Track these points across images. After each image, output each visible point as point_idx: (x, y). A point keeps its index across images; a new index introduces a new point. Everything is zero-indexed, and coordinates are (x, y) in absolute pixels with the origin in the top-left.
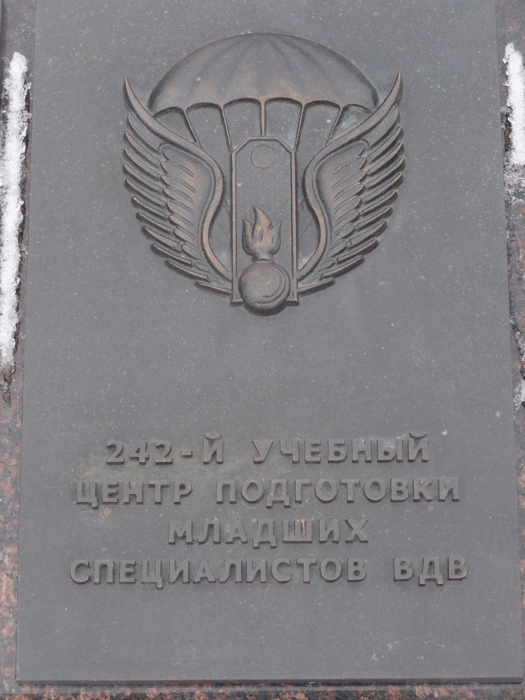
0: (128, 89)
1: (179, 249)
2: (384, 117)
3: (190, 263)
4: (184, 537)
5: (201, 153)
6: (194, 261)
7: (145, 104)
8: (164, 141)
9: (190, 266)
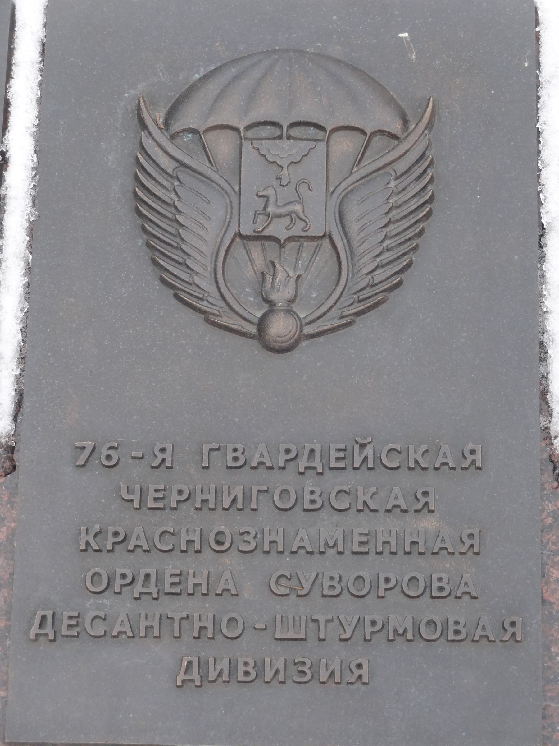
0: (145, 115)
1: (190, 281)
2: (413, 144)
3: (201, 296)
4: (335, 544)
5: (215, 177)
6: (206, 295)
9: (202, 299)
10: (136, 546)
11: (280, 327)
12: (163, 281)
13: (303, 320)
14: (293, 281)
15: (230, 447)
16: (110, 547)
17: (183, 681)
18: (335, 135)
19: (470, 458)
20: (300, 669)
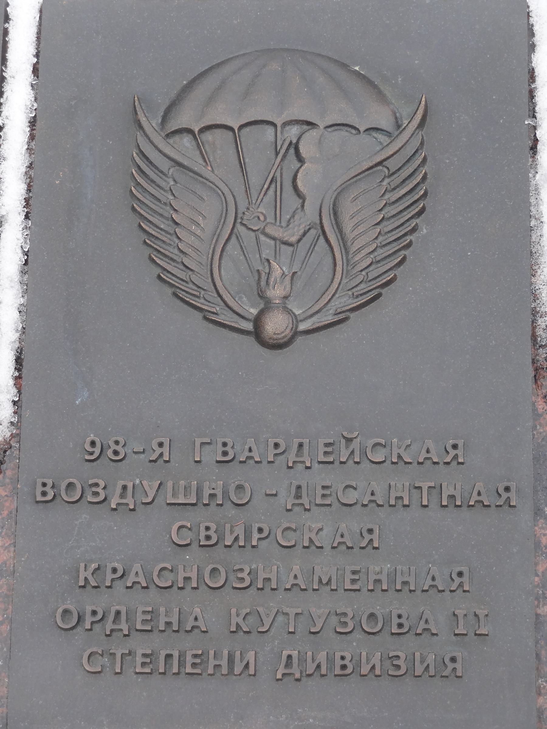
6: (203, 292)
7: (156, 122)
9: (198, 297)
11: (276, 325)
13: (298, 317)
14: (288, 279)
15: (220, 441)
17: (284, 675)
19: (452, 452)
20: (394, 663)
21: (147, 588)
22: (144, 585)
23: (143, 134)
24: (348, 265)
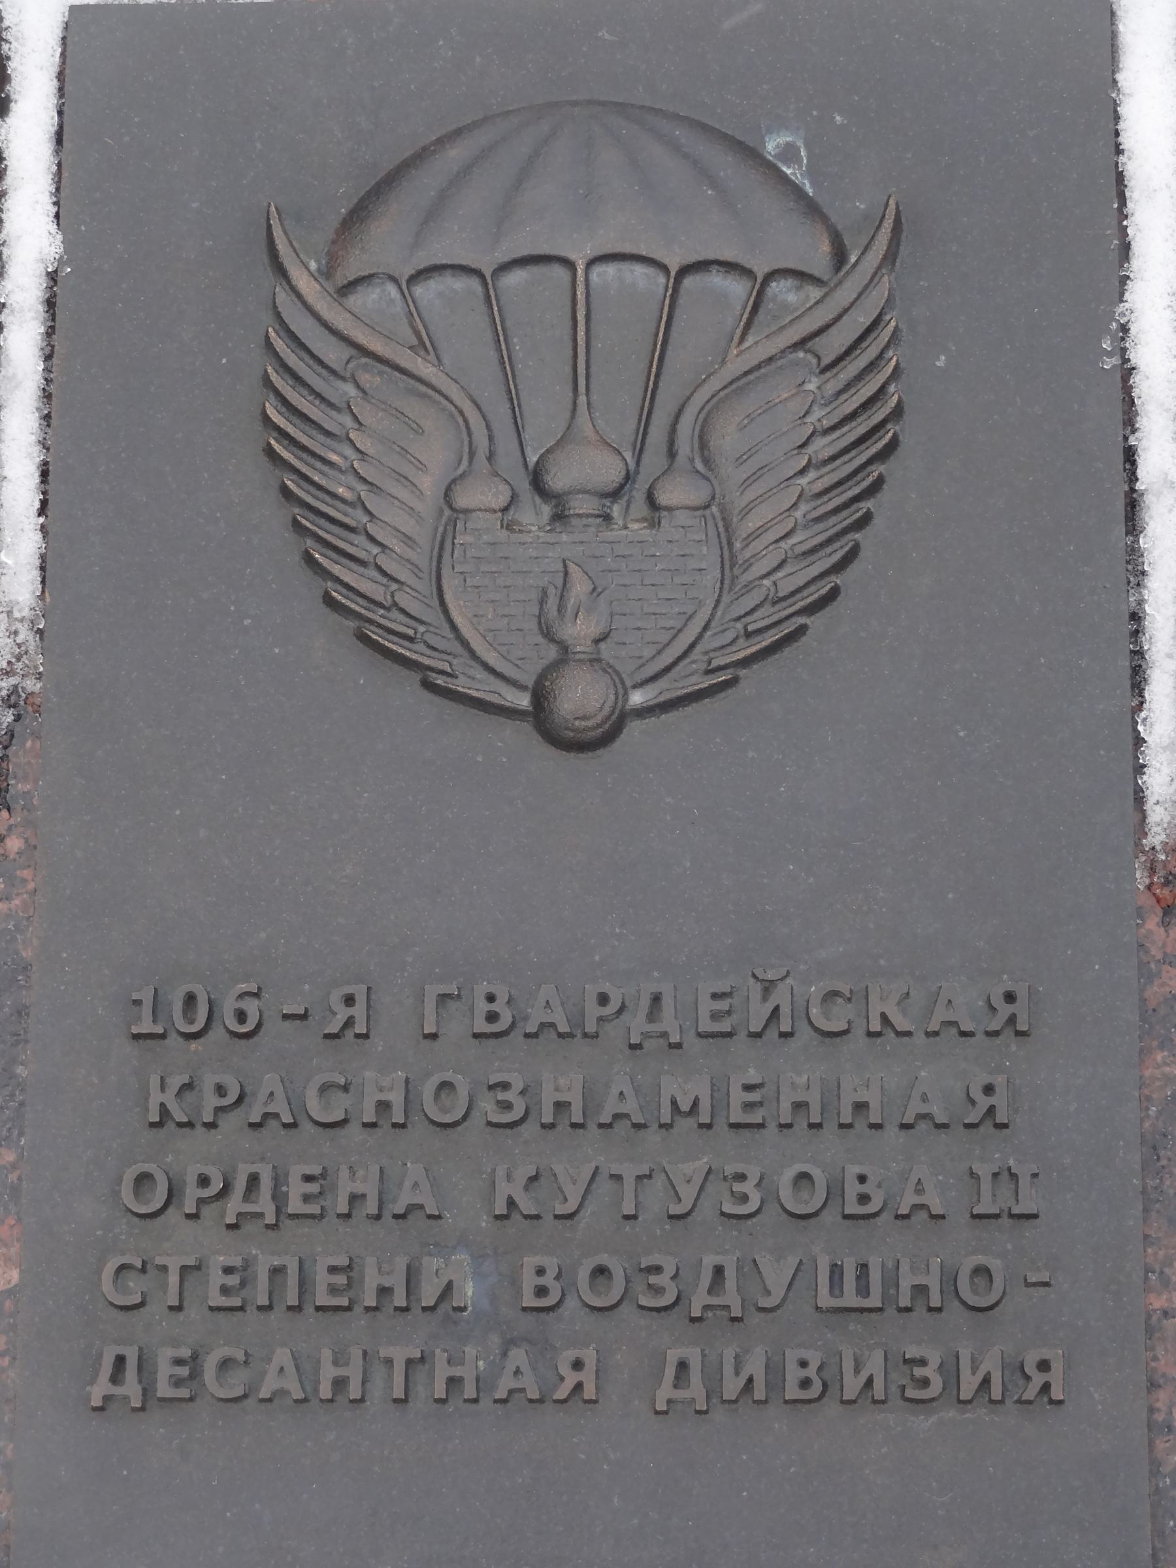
0: (278, 233)
1: (388, 602)
3: (411, 632)
6: (422, 629)
8: (354, 352)
9: (411, 639)
10: (266, 1115)
11: (581, 697)
12: (329, 601)
16: (208, 1117)
18: (689, 282)
21: (294, 1125)
22: (287, 1119)
23: (287, 288)
24: (732, 567)
